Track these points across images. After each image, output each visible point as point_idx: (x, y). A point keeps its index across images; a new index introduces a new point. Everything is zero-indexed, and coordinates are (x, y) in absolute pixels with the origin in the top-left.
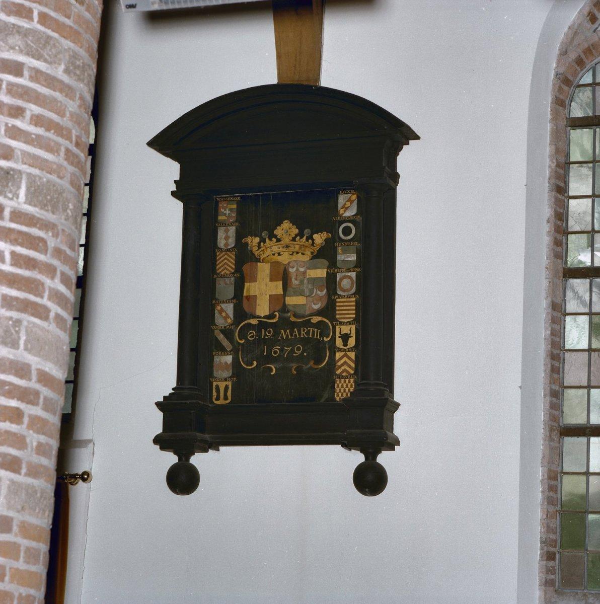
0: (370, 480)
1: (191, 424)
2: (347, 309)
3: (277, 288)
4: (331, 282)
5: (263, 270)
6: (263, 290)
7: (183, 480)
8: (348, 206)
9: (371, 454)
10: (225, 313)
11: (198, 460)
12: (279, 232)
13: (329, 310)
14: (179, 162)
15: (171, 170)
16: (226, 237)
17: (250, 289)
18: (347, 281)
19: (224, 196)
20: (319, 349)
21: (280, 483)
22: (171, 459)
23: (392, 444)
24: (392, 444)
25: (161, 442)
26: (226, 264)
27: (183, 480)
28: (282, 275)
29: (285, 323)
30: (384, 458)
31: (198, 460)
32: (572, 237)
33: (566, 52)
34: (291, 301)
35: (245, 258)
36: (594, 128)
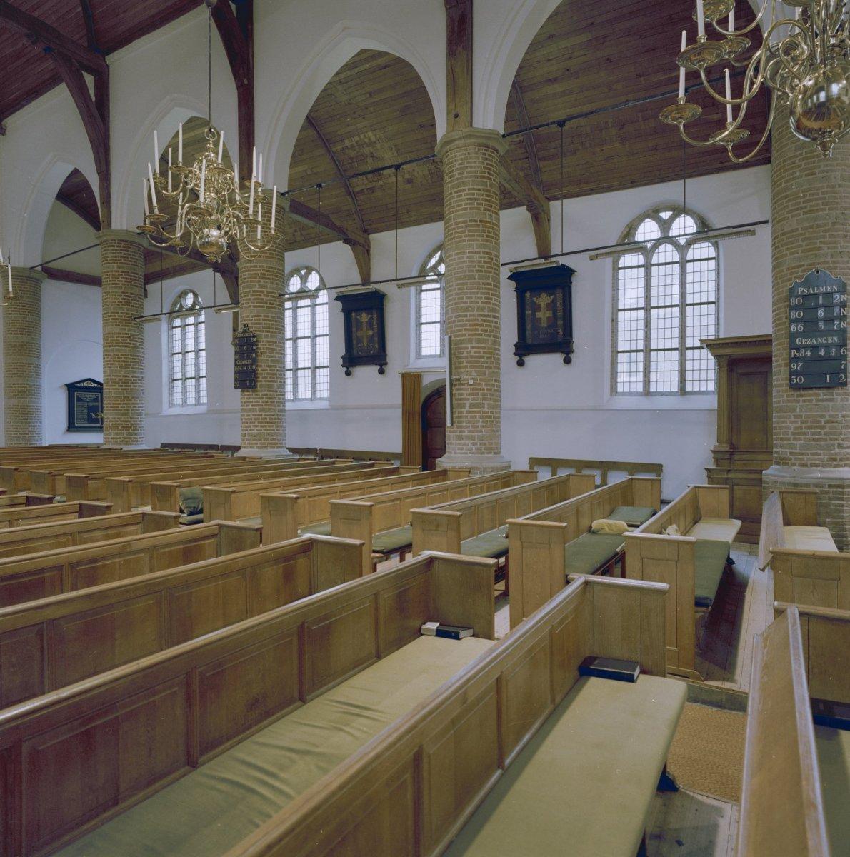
1: (524, 349)
7: (521, 363)
12: (541, 296)
15: (513, 284)
22: (517, 358)
25: (343, 366)
27: (521, 363)
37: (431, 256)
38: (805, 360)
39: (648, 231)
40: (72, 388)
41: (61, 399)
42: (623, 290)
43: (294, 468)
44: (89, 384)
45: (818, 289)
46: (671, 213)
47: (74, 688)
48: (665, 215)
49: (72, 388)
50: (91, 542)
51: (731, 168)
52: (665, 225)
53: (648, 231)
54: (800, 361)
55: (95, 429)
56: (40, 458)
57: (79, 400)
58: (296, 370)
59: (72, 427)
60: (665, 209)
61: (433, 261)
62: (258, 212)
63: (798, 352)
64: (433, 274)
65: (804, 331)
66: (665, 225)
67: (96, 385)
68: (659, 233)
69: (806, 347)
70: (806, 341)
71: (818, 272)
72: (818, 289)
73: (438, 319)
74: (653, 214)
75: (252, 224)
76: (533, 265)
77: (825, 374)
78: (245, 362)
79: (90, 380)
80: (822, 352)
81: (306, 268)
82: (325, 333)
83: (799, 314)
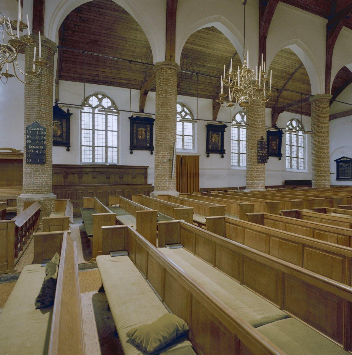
0: (68, 150)
2: (220, 142)
3: (215, 140)
4: (219, 139)
5: (213, 138)
6: (213, 139)
7: (131, 153)
8: (220, 133)
9: (223, 154)
10: (210, 141)
11: (209, 154)
13: (219, 142)
14: (97, 256)
16: (210, 134)
17: (61, 132)
18: (220, 139)
19: (175, 271)
20: (218, 145)
21: (215, 157)
23: (225, 153)
24: (225, 153)
26: (210, 137)
27: (131, 153)
28: (215, 138)
29: (215, 143)
30: (224, 155)
31: (209, 154)
32: (136, 93)
33: (329, 90)
34: (216, 141)
35: (212, 137)
36: (214, 123)
37: (188, 109)
38: (32, 154)
39: (93, 101)
40: (337, 161)
41: (335, 164)
42: (241, 139)
43: (224, 194)
44: (344, 159)
45: (37, 129)
46: (98, 96)
47: (337, 283)
48: (100, 96)
49: (337, 161)
50: (338, 226)
51: (102, 83)
52: (100, 100)
53: (93, 101)
54: (30, 154)
55: (349, 179)
56: (301, 191)
57: (341, 166)
58: (291, 157)
59: (338, 179)
60: (100, 94)
61: (186, 109)
62: (36, 52)
63: (29, 150)
64: (101, 107)
65: (31, 143)
66: (100, 100)
67: (347, 159)
68: (98, 102)
69: (32, 149)
70: (32, 147)
71: (36, 123)
72: (37, 129)
73: (245, 140)
74: (96, 95)
75: (261, 90)
76: (141, 115)
77: (37, 159)
78: (263, 152)
79: (343, 157)
80: (37, 152)
81: (103, 95)
82: (293, 146)
83: (29, 137)
